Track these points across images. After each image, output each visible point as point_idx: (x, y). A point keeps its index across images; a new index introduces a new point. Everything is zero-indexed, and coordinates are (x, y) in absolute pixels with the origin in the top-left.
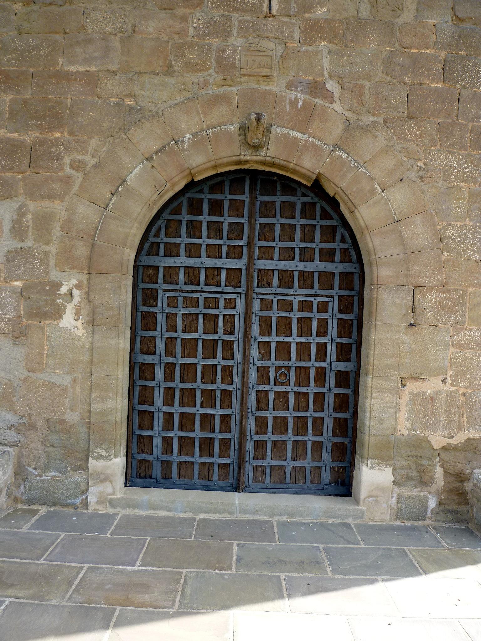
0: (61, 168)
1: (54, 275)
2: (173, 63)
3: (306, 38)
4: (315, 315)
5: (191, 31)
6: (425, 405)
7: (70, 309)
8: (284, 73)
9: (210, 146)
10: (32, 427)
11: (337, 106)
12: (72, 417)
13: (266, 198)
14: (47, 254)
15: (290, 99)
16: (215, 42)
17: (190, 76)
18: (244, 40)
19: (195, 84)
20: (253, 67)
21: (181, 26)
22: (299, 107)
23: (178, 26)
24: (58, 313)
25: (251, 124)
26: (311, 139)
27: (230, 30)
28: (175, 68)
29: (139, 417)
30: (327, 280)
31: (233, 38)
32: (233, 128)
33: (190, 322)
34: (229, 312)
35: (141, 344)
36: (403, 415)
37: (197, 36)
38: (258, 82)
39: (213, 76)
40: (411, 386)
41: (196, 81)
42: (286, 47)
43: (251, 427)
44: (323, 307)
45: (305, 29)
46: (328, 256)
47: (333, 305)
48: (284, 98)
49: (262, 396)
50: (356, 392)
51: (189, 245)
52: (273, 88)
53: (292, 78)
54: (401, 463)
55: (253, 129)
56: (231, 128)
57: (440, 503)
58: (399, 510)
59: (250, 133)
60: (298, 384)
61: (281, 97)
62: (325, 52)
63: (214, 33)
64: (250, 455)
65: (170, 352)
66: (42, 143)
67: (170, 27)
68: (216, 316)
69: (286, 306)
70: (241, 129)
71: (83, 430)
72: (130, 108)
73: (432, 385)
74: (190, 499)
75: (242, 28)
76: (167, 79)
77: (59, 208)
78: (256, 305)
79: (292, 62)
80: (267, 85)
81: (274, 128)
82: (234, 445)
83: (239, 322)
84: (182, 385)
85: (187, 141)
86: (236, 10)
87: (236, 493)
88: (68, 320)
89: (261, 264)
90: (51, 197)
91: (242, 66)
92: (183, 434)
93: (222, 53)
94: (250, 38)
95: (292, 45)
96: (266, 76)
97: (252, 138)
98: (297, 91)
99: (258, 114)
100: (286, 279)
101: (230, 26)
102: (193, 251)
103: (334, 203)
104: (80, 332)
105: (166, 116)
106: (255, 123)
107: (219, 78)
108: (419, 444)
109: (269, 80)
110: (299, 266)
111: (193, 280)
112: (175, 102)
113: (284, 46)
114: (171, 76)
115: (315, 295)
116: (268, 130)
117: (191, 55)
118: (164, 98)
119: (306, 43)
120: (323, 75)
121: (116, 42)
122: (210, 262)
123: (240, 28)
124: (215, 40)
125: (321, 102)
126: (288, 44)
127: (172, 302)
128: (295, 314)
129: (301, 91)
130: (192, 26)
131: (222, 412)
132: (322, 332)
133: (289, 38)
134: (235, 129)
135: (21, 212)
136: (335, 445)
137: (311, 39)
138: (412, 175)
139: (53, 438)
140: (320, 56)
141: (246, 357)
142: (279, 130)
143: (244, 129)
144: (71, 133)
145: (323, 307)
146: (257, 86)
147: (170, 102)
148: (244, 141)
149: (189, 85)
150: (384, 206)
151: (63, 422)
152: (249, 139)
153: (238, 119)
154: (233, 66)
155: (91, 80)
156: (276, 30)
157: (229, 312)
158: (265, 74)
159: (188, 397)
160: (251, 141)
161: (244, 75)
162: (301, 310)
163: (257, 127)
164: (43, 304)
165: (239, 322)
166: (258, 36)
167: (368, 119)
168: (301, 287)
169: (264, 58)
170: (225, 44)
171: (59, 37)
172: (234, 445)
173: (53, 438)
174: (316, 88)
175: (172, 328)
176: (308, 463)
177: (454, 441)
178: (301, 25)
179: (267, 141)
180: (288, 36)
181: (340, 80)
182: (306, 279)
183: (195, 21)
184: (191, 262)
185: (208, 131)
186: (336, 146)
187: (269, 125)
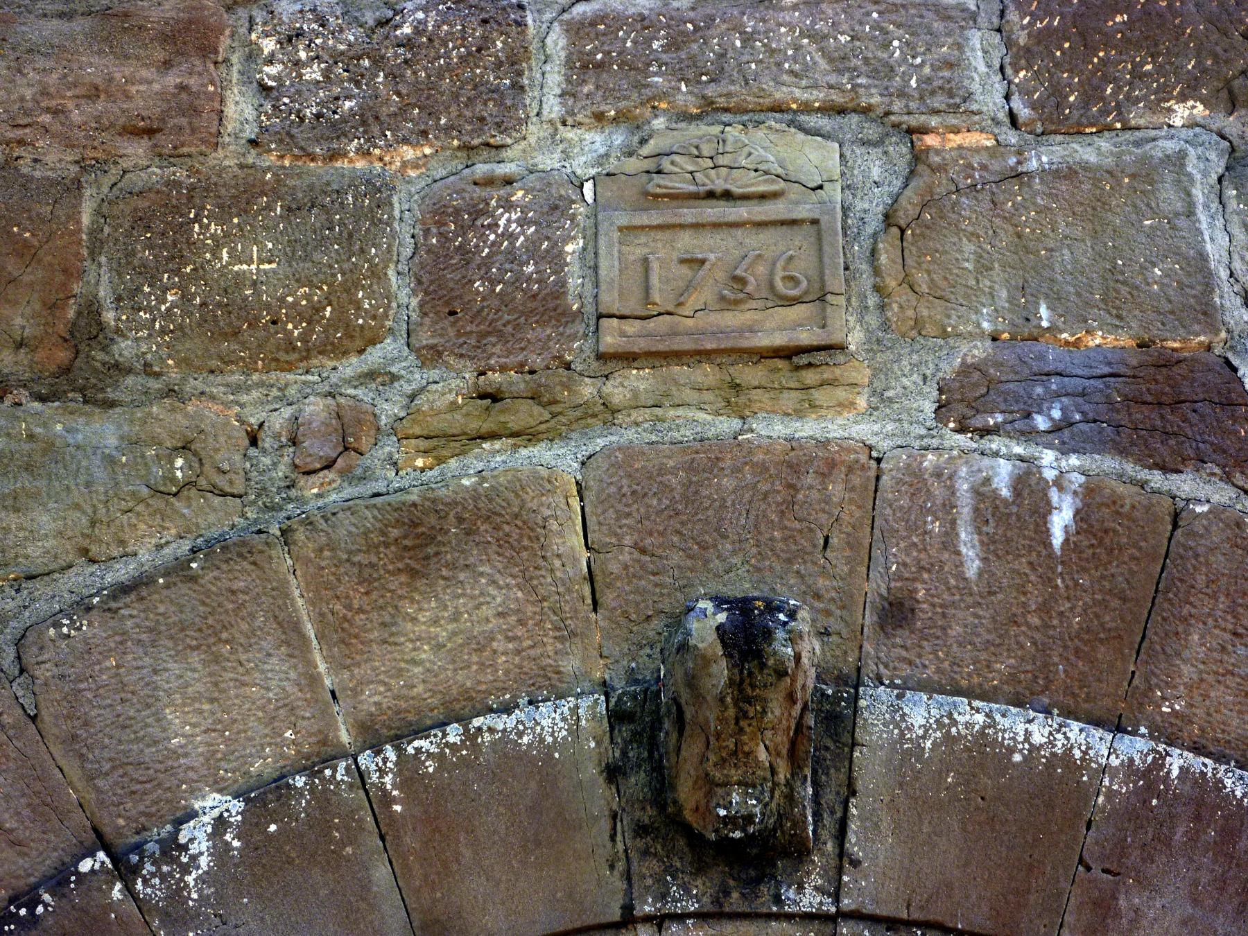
2: (109, 316)
3: (1058, 93)
5: (241, 110)
8: (918, 324)
9: (381, 873)
15: (983, 491)
16: (412, 167)
17: (237, 389)
18: (619, 139)
19: (267, 443)
20: (693, 302)
21: (172, 80)
22: (1058, 538)
23: (149, 84)
25: (692, 682)
26: (1177, 761)
27: (518, 88)
28: (125, 349)
31: (534, 131)
37: (286, 139)
38: (734, 397)
39: (403, 378)
41: (279, 421)
42: (918, 157)
45: (1045, 39)
48: (938, 490)
52: (847, 425)
53: (979, 351)
55: (711, 715)
56: (549, 720)
59: (692, 749)
61: (915, 479)
62: (1204, 165)
63: (403, 111)
67: (94, 93)
70: (625, 731)
74: (893, 284)
75: (599, 66)
76: (58, 423)
79: (969, 247)
80: (799, 414)
81: (875, 704)
85: (202, 845)
91: (610, 301)
93: (462, 230)
94: (659, 123)
95: (956, 140)
96: (788, 353)
97: (710, 785)
98: (1029, 435)
99: (741, 607)
101: (514, 61)
105: (43, 673)
106: (721, 672)
109: (810, 377)
112: (122, 572)
113: (899, 150)
114: (98, 400)
116: (831, 724)
117: (236, 258)
118: (35, 554)
119: (1055, 121)
120: (1208, 315)
123: (582, 66)
124: (408, 153)
125: (1222, 494)
126: (931, 140)
129: (1056, 429)
130: (246, 78)
133: (938, 102)
134: (575, 730)
137: (1091, 94)
140: (1168, 197)
142: (920, 713)
143: (644, 723)
146: (726, 425)
147: (81, 579)
148: (647, 815)
149: (230, 455)
152: (686, 793)
153: (596, 658)
154: (549, 306)
156: (839, 62)
158: (779, 340)
160: (705, 811)
161: (629, 358)
163: (744, 694)
166: (709, 109)
169: (766, 236)
170: (481, 169)
178: (1013, 15)
179: (829, 797)
180: (928, 89)
183: (269, 45)
185: (365, 760)
187: (841, 680)
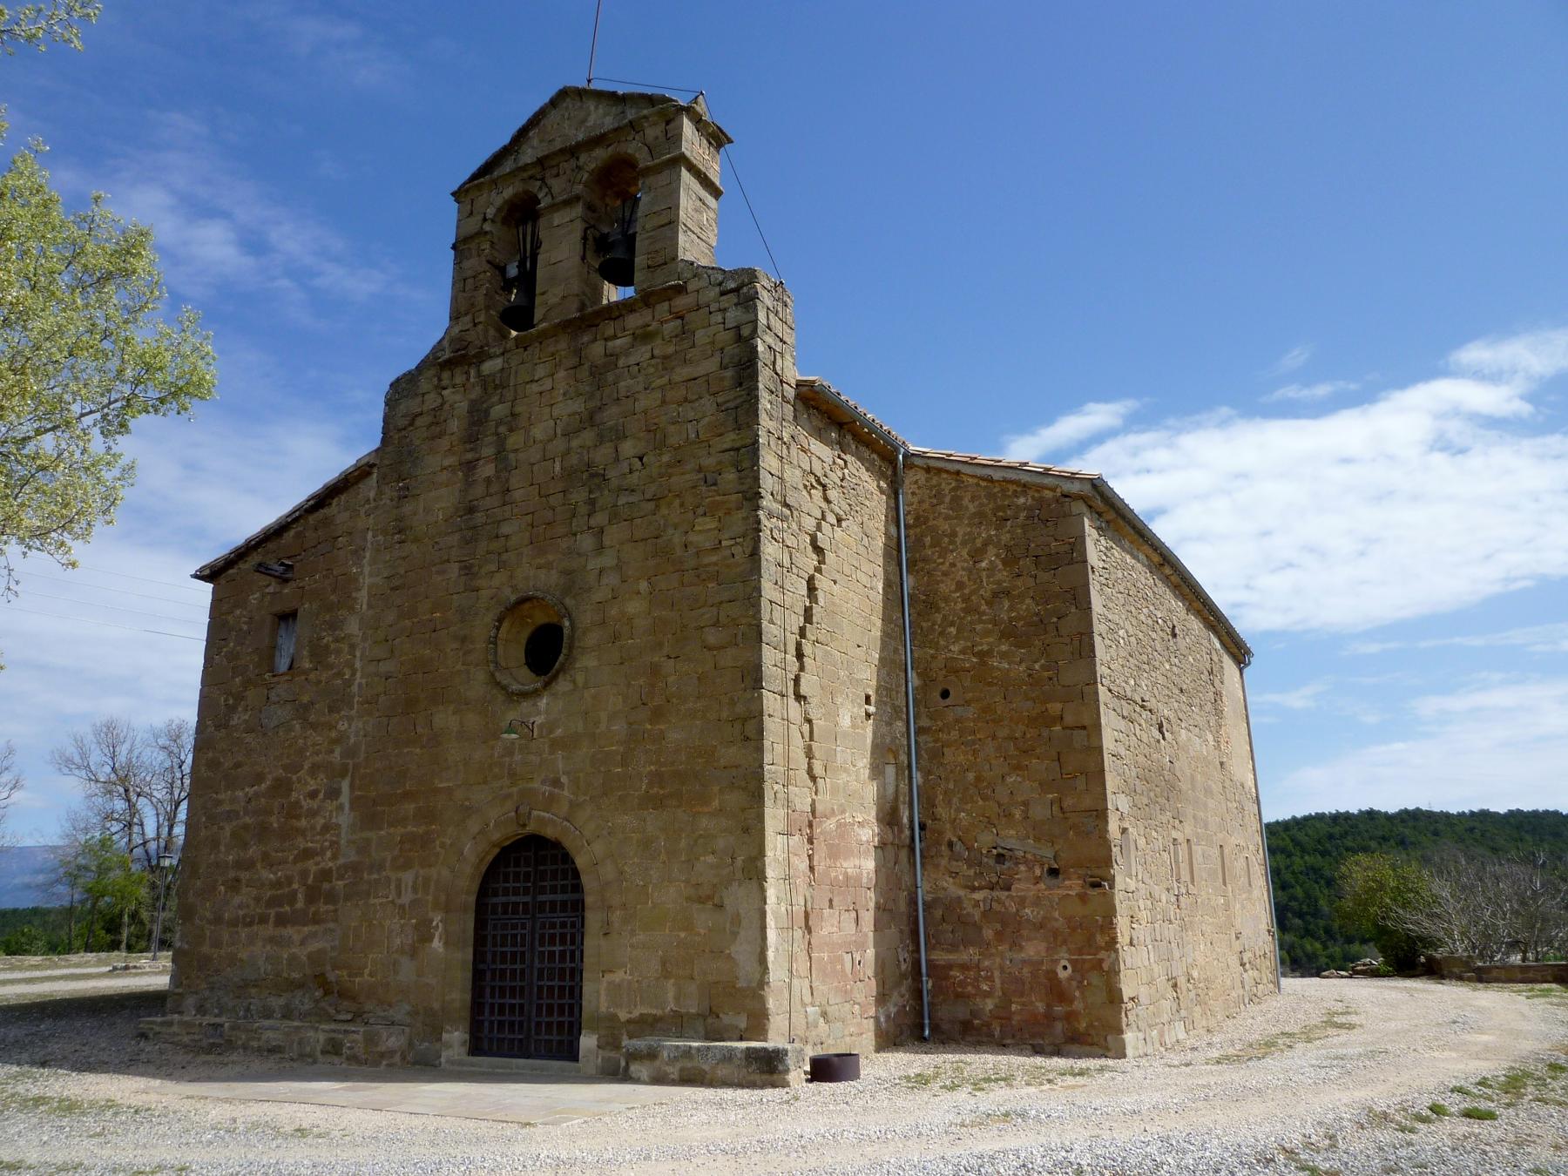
10: (417, 1013)
11: (566, 793)
12: (436, 1006)
24: (431, 939)
29: (477, 1007)
35: (478, 956)
40: (608, 977)
69: (553, 926)
108: (613, 1018)
110: (559, 897)
128: (558, 931)
132: (494, 937)
167: (581, 799)
174: (556, 783)
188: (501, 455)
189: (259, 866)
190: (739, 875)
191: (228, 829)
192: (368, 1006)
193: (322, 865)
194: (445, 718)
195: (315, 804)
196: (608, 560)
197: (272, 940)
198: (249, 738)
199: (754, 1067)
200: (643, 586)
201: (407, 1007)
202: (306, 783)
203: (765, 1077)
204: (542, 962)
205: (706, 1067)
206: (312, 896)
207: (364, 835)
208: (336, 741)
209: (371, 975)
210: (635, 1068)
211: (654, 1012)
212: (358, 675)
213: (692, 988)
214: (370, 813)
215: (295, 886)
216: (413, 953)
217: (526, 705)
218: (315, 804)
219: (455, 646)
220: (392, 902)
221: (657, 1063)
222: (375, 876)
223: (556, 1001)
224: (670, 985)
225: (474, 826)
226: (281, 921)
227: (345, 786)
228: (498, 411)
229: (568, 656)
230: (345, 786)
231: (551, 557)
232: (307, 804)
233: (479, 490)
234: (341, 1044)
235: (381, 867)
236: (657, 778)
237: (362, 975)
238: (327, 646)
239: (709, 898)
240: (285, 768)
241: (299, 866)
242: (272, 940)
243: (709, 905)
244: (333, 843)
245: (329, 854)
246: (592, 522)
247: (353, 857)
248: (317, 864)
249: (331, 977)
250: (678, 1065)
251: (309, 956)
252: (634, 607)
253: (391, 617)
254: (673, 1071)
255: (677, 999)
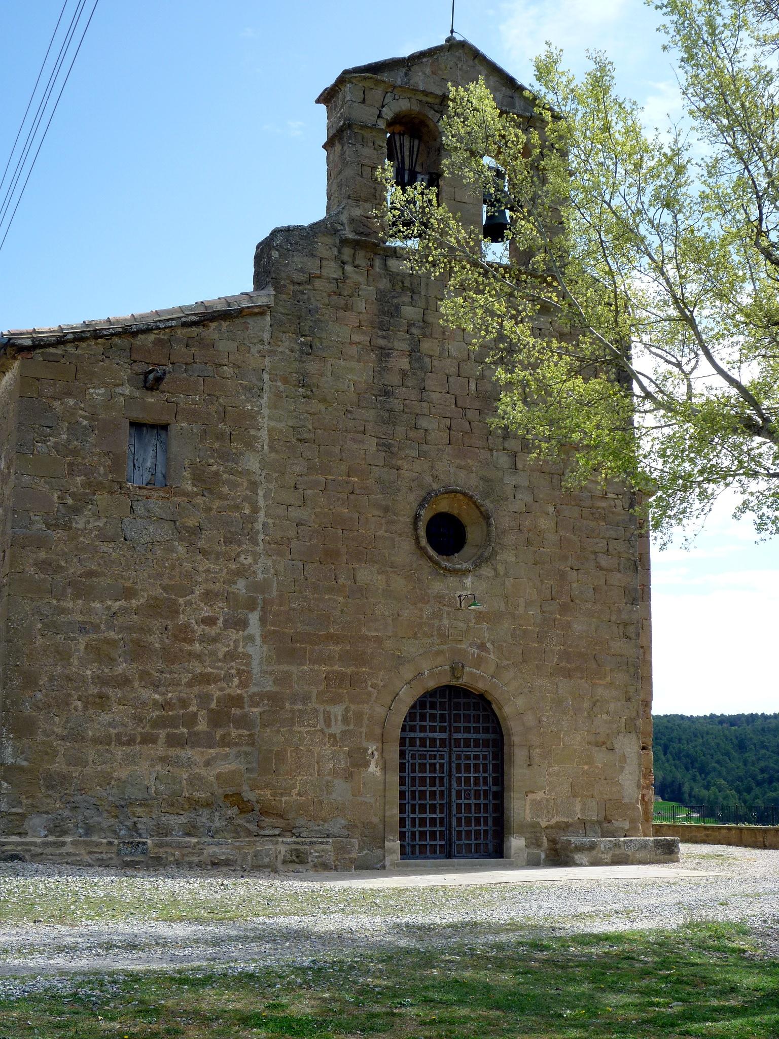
0: (366, 687)
1: (365, 744)
4: (481, 761)
6: (536, 804)
7: (373, 761)
10: (355, 826)
11: (492, 656)
12: (375, 820)
13: (456, 700)
14: (361, 733)
16: (436, 622)
24: (367, 764)
30: (486, 743)
32: (447, 667)
33: (423, 767)
34: (442, 761)
36: (528, 811)
40: (530, 796)
43: (454, 823)
44: (485, 758)
46: (486, 730)
47: (490, 757)
49: (459, 806)
50: (502, 803)
51: (420, 726)
52: (463, 646)
54: (528, 835)
57: (546, 856)
58: (528, 861)
60: (475, 799)
64: (455, 838)
65: (413, 784)
66: (356, 674)
68: (435, 764)
69: (468, 757)
71: (381, 826)
72: (399, 657)
73: (539, 796)
77: (365, 708)
78: (454, 757)
82: (446, 834)
83: (446, 766)
84: (420, 802)
86: (445, 605)
87: (653, 703)
88: (372, 768)
89: (456, 736)
90: (362, 702)
92: (421, 829)
100: (467, 743)
102: (423, 729)
103: (489, 703)
104: (379, 774)
107: (439, 641)
110: (473, 736)
111: (423, 744)
115: (480, 751)
119: (477, 624)
121: (390, 620)
122: (431, 735)
123: (447, 615)
127: (413, 757)
128: (472, 762)
131: (440, 816)
132: (485, 771)
135: (347, 710)
136: (494, 831)
138: (526, 690)
139: (366, 832)
141: (450, 785)
143: (453, 669)
144: (370, 669)
145: (485, 758)
150: (515, 704)
151: (371, 823)
155: (379, 640)
157: (442, 761)
159: (423, 808)
162: (475, 759)
164: (358, 760)
165: (446, 766)
167: (506, 662)
168: (475, 747)
171: (362, 616)
172: (446, 834)
173: (366, 832)
174: (482, 647)
175: (413, 771)
176: (481, 841)
177: (551, 823)
181: (492, 642)
182: (477, 743)
184: (422, 735)
186: (492, 677)
188: (414, 353)
189: (136, 684)
190: (623, 729)
191: (82, 641)
192: (301, 821)
193: (227, 691)
194: (366, 575)
195: (213, 631)
196: (522, 480)
197: (163, 760)
198: (105, 547)
199: (660, 851)
200: (551, 509)
201: (344, 822)
202: (198, 609)
203: (666, 857)
204: (459, 784)
205: (630, 853)
206: (217, 719)
207: (285, 667)
208: (239, 573)
209: (299, 794)
210: (577, 857)
211: (566, 820)
212: (262, 514)
213: (593, 804)
214: (286, 648)
215: (194, 709)
216: (349, 776)
217: (452, 581)
218: (213, 631)
219: (377, 513)
220: (322, 731)
221: (595, 852)
222: (299, 707)
223: (473, 815)
224: (577, 801)
225: (407, 673)
226: (174, 741)
227: (254, 618)
228: (409, 312)
229: (430, 558)
230: (254, 618)
231: (470, 463)
232: (199, 629)
233: (395, 379)
234: (307, 854)
235: (305, 699)
236: (565, 655)
237: (290, 795)
238: (217, 474)
239: (604, 743)
240: (165, 588)
241: (196, 689)
242: (163, 760)
243: (604, 748)
244: (239, 673)
245: (236, 681)
246: (506, 445)
247: (269, 686)
248: (222, 689)
249: (249, 795)
250: (611, 854)
251: (218, 777)
252: (545, 524)
253: (299, 467)
254: (607, 857)
255: (583, 810)
